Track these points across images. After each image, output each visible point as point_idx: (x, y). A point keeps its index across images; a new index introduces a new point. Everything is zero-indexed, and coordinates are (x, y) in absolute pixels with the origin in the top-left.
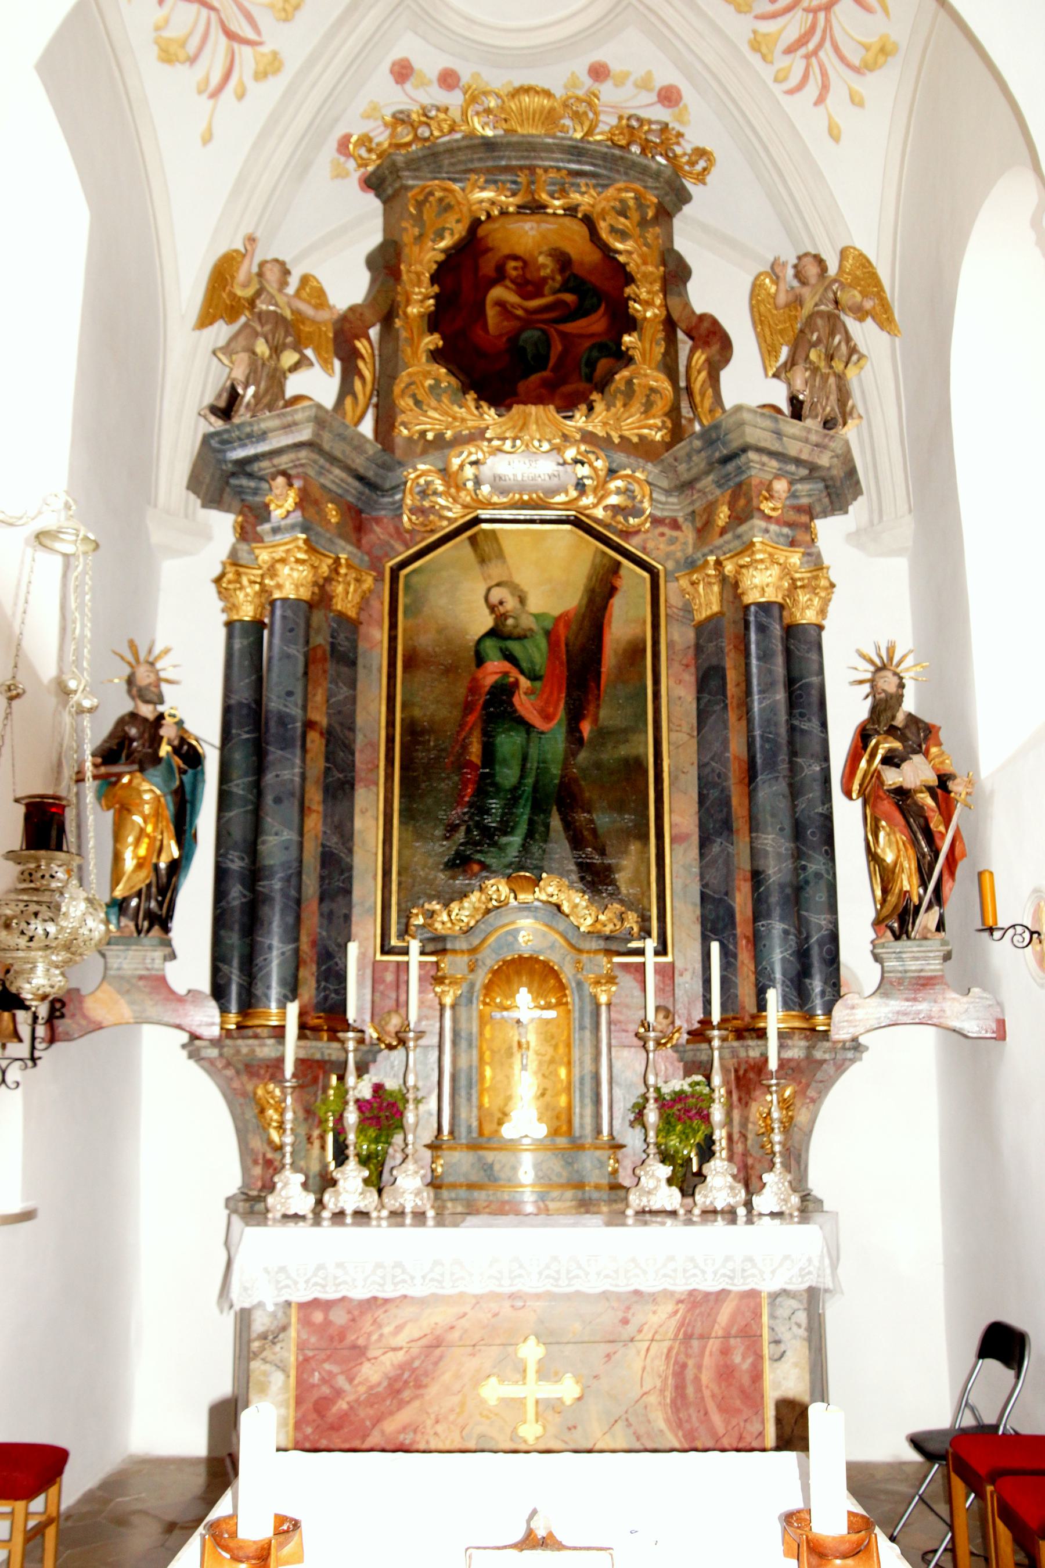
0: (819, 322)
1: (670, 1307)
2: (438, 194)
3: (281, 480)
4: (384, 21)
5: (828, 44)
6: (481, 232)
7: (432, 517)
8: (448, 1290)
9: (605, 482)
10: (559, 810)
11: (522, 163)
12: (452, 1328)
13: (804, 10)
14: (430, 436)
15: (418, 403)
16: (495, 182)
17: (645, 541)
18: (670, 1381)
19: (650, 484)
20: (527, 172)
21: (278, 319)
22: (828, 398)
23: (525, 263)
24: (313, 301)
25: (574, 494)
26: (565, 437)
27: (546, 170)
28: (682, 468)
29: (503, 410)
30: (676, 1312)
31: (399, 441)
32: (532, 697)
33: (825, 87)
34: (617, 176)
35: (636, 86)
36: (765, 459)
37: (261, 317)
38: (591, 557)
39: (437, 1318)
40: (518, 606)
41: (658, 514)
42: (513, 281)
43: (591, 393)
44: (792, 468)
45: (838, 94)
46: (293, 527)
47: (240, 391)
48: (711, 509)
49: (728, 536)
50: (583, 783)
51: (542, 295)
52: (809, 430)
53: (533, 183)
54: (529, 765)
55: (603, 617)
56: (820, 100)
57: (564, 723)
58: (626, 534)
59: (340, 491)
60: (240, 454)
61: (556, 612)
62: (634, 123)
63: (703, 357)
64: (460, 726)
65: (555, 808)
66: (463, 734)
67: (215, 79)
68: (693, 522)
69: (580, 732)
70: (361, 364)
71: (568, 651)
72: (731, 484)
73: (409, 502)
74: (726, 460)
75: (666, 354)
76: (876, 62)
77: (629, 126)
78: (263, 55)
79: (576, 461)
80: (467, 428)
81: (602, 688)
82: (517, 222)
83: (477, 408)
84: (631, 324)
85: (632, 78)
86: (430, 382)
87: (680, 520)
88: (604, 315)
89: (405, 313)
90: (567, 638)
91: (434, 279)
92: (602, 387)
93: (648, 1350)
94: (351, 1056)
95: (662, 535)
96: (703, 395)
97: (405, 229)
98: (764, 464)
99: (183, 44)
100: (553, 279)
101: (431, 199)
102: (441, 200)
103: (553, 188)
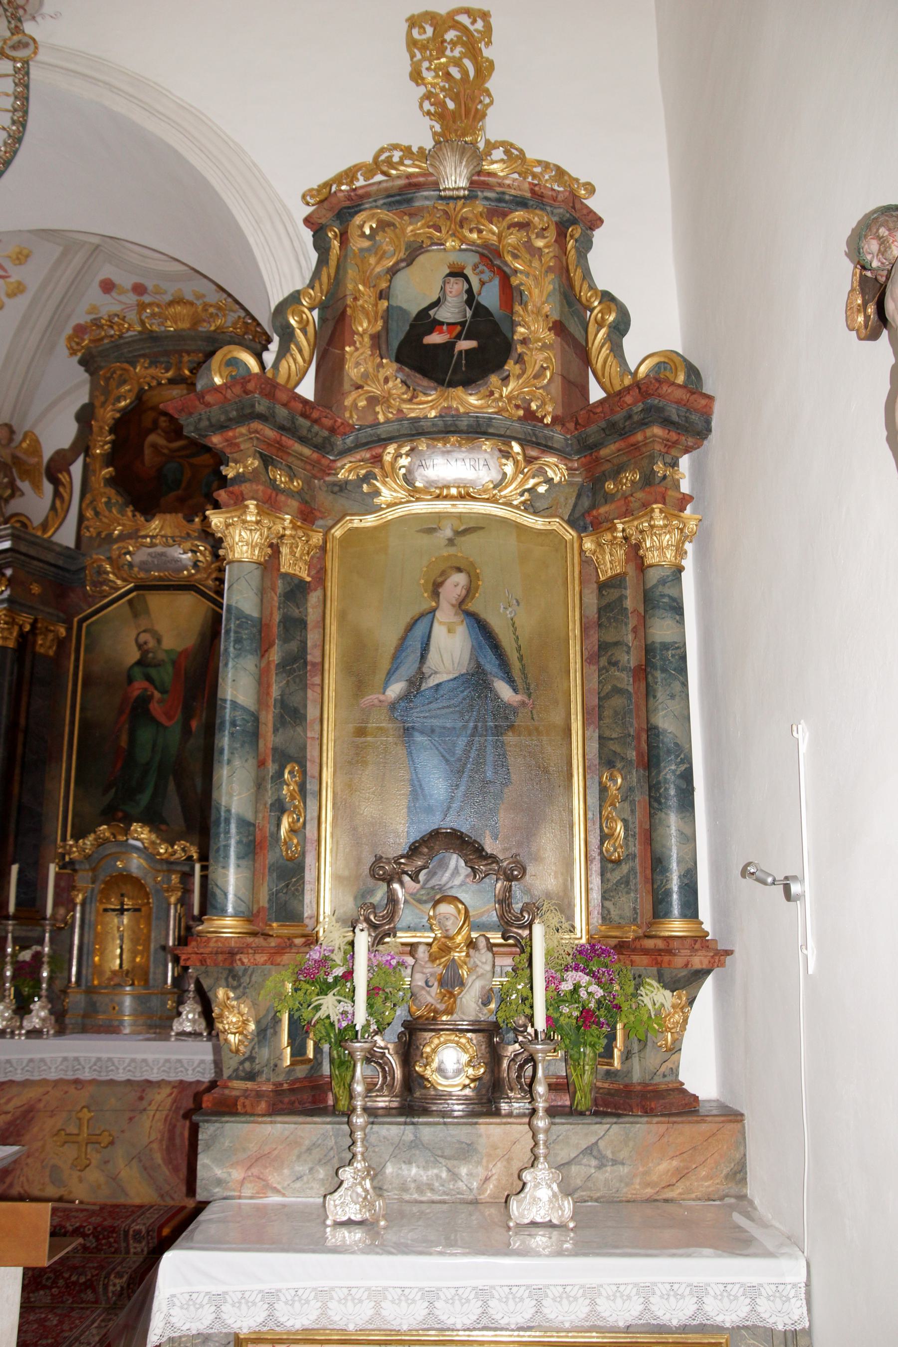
1: (168, 1090)
4: (88, 259)
6: (145, 398)
8: (36, 1077)
12: (40, 1100)
14: (103, 535)
18: (166, 1135)
20: (177, 355)
30: (171, 1094)
39: (30, 1094)
61: (179, 649)
78: (12, 283)
86: (104, 500)
91: (111, 431)
93: (154, 1116)
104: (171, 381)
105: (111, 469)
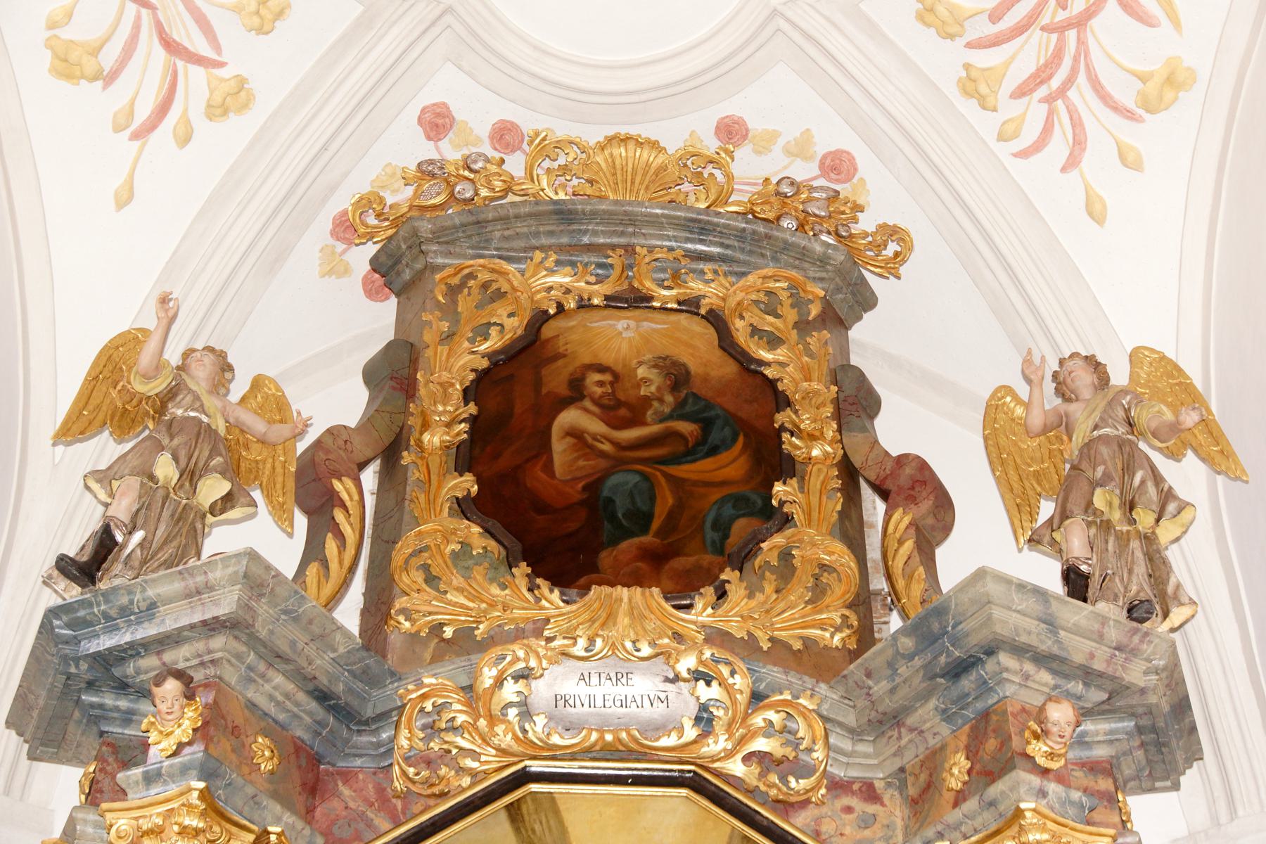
0: (1104, 451)
2: (484, 276)
3: (172, 687)
5: (1082, 78)
6: (548, 331)
7: (443, 771)
9: (746, 716)
11: (615, 240)
13: (1043, 29)
14: (448, 632)
15: (431, 580)
16: (573, 264)
17: (818, 821)
19: (825, 719)
21: (203, 432)
22: (1130, 571)
23: (616, 377)
25: (691, 733)
26: (678, 637)
27: (651, 250)
28: (880, 688)
29: (573, 592)
31: (394, 639)
33: (1079, 143)
34: (760, 261)
35: (788, 152)
36: (1029, 667)
37: (172, 427)
41: (839, 772)
42: (596, 402)
43: (722, 570)
44: (1077, 687)
45: (1099, 152)
46: (184, 770)
47: (119, 538)
48: (934, 761)
49: (971, 805)
51: (643, 423)
52: (1104, 621)
53: (631, 267)
56: (1071, 163)
58: (785, 806)
59: (282, 717)
60: (106, 642)
62: (786, 189)
63: (907, 520)
67: (144, 111)
68: (903, 786)
70: (339, 515)
72: (969, 713)
73: (404, 743)
74: (959, 670)
75: (842, 514)
76: (1161, 98)
77: (778, 194)
78: (222, 80)
79: (697, 676)
80: (512, 620)
82: (604, 319)
83: (530, 590)
84: (786, 467)
85: (781, 142)
87: (879, 785)
88: (745, 446)
89: (419, 443)
91: (467, 395)
92: (741, 560)
95: (849, 810)
96: (909, 578)
97: (430, 323)
98: (1027, 677)
99: (95, 52)
100: (661, 400)
101: (471, 283)
102: (485, 286)
103: (662, 276)
104: (612, 301)
105: (469, 477)
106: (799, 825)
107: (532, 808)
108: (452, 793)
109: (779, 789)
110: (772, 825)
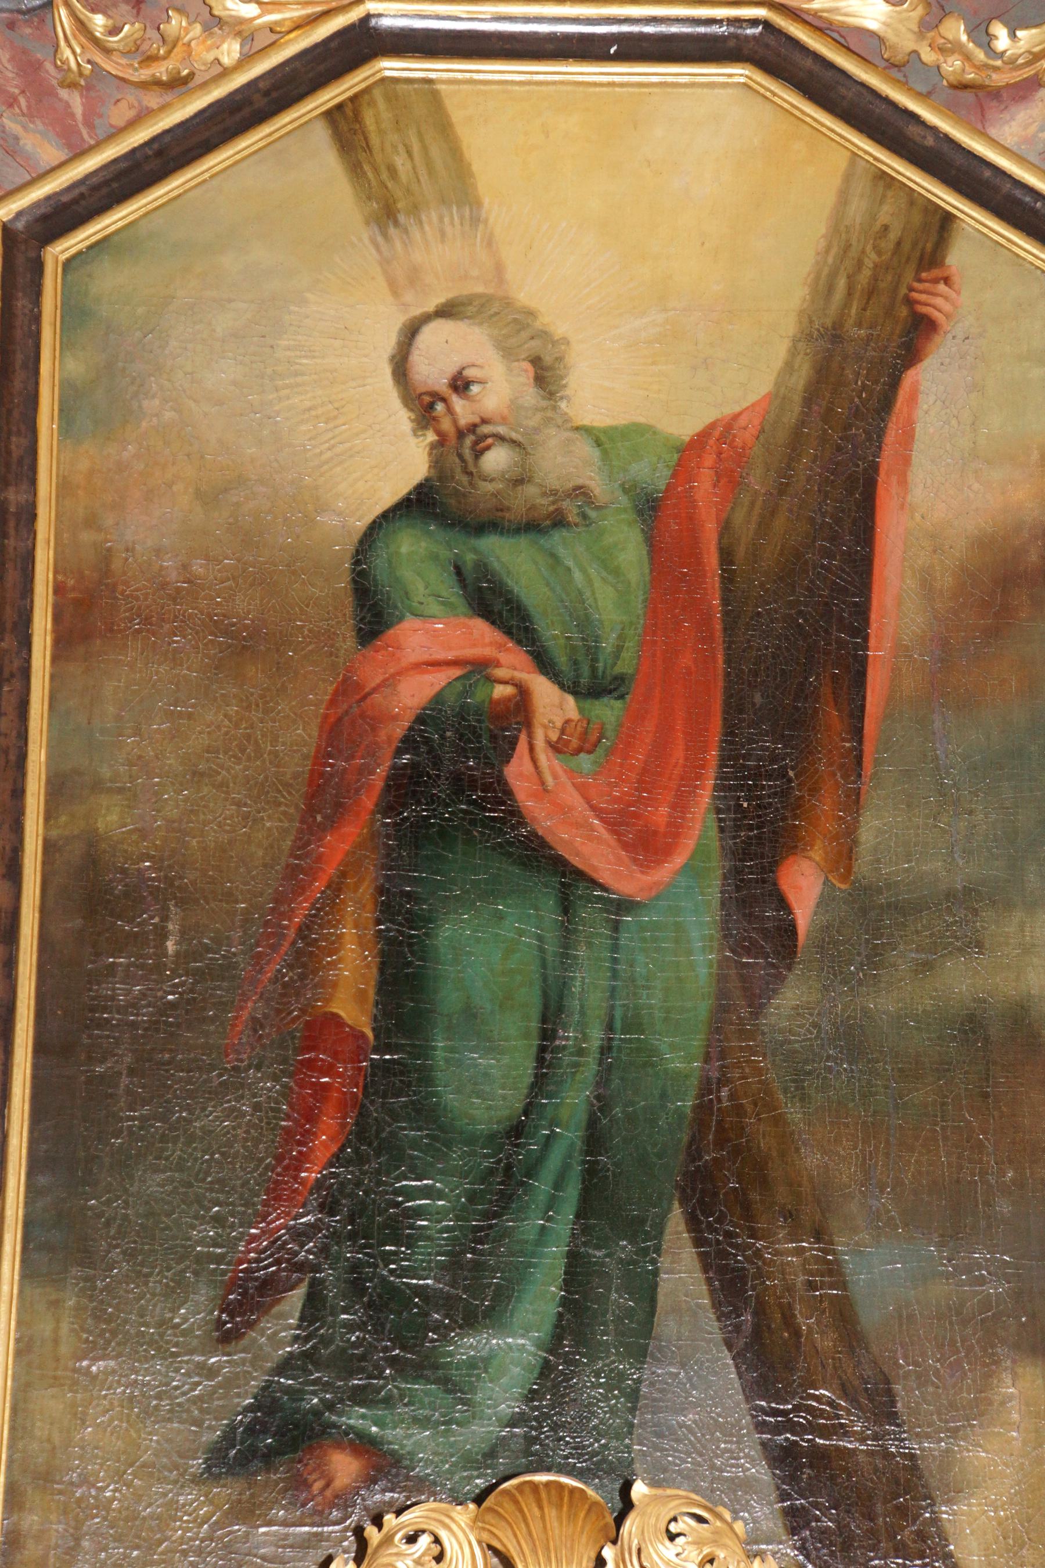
10: (693, 1223)
24: (357, 126)
32: (585, 761)
38: (829, 199)
40: (530, 396)
50: (794, 1113)
54: (568, 1036)
55: (876, 437)
57: (716, 867)
64: (292, 872)
65: (676, 1220)
66: (302, 909)
69: (783, 904)
71: (728, 579)
81: (869, 726)
90: (726, 528)
94: (145, 1457)
106: (1009, 141)
107: (386, 115)
108: (198, 80)
109: (967, 57)
110: (946, 147)
